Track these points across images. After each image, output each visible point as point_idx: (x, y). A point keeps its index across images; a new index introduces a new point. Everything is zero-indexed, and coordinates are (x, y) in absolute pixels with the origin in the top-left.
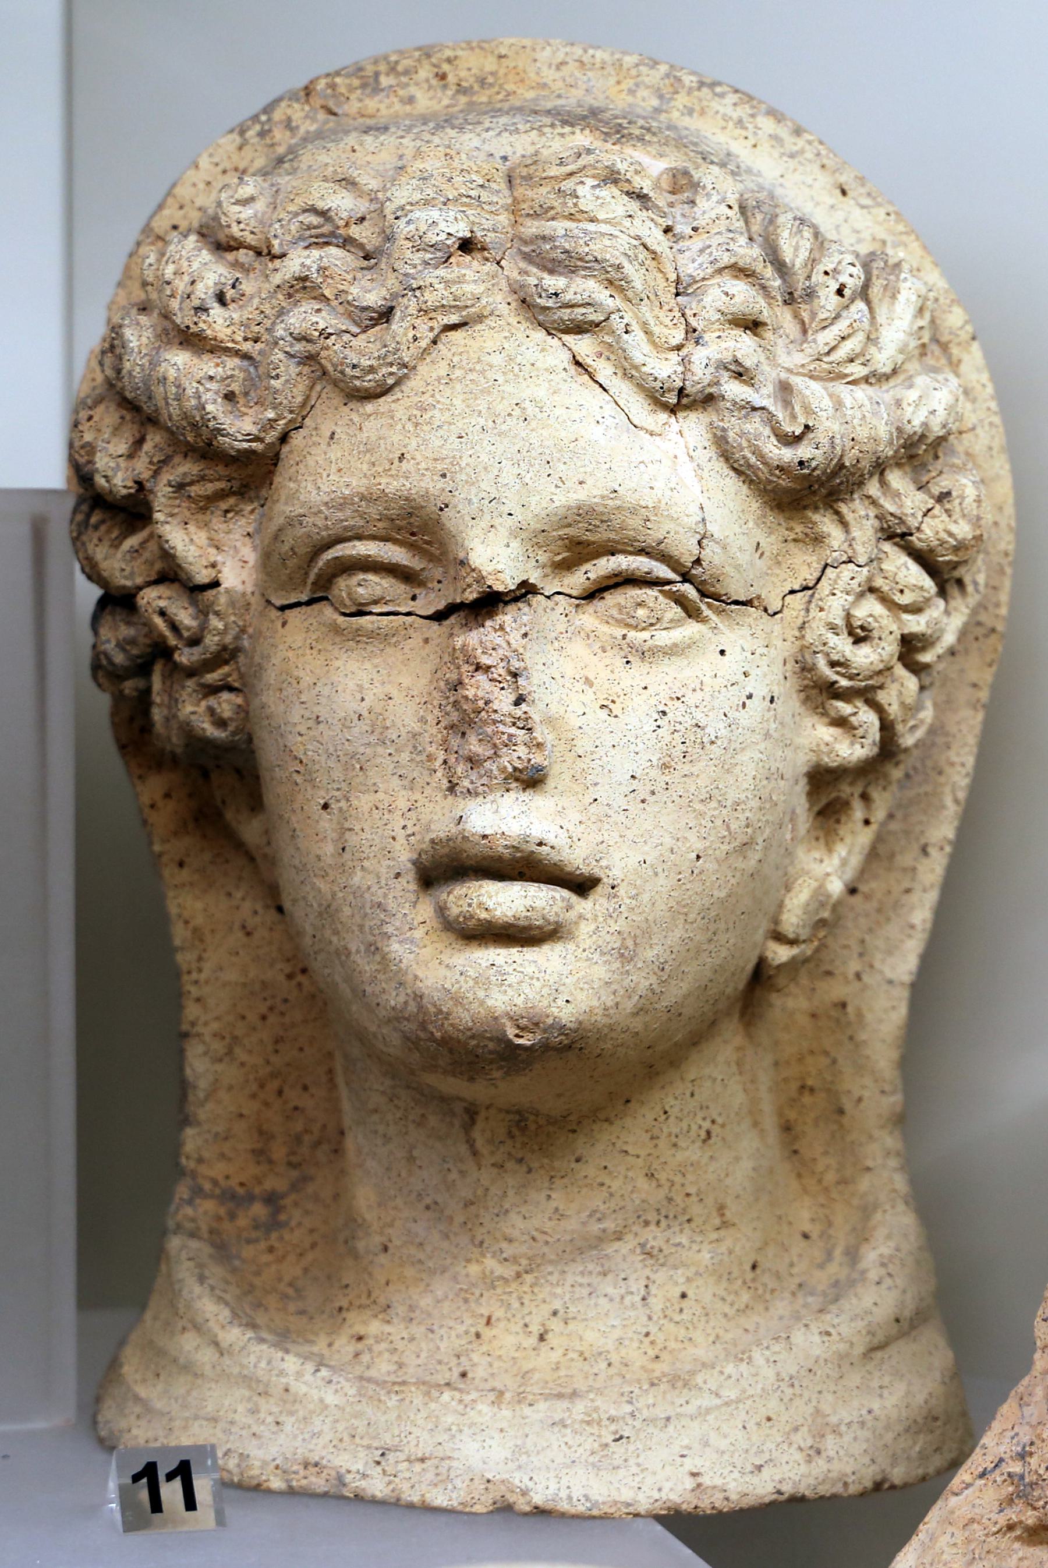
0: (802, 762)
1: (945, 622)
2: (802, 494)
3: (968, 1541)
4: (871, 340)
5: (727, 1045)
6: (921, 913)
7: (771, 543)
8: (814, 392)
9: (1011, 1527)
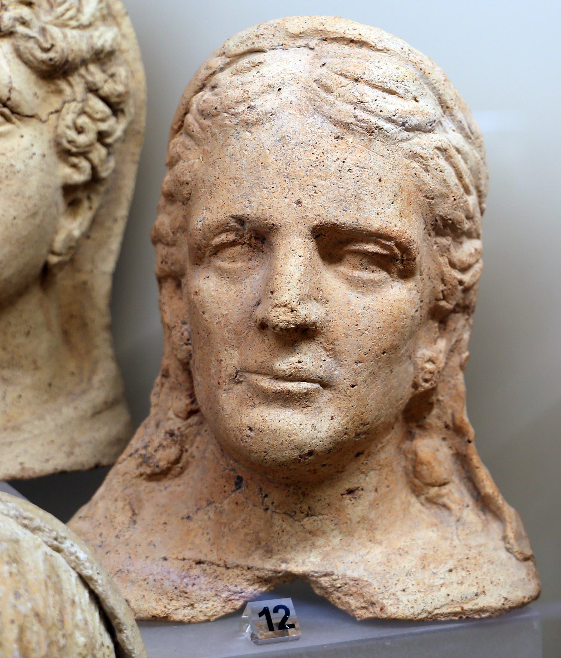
0: (59, 182)
1: (117, 127)
2: (53, 72)
3: (124, 481)
4: (79, 11)
5: (35, 298)
6: (115, 244)
7: (41, 93)
8: (56, 32)
9: (141, 475)
